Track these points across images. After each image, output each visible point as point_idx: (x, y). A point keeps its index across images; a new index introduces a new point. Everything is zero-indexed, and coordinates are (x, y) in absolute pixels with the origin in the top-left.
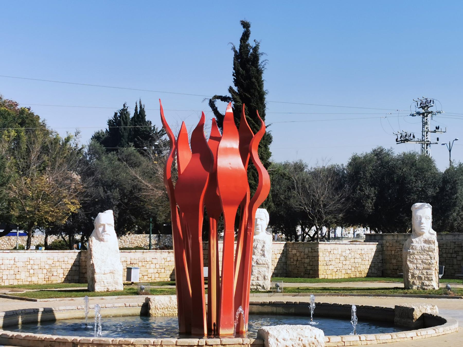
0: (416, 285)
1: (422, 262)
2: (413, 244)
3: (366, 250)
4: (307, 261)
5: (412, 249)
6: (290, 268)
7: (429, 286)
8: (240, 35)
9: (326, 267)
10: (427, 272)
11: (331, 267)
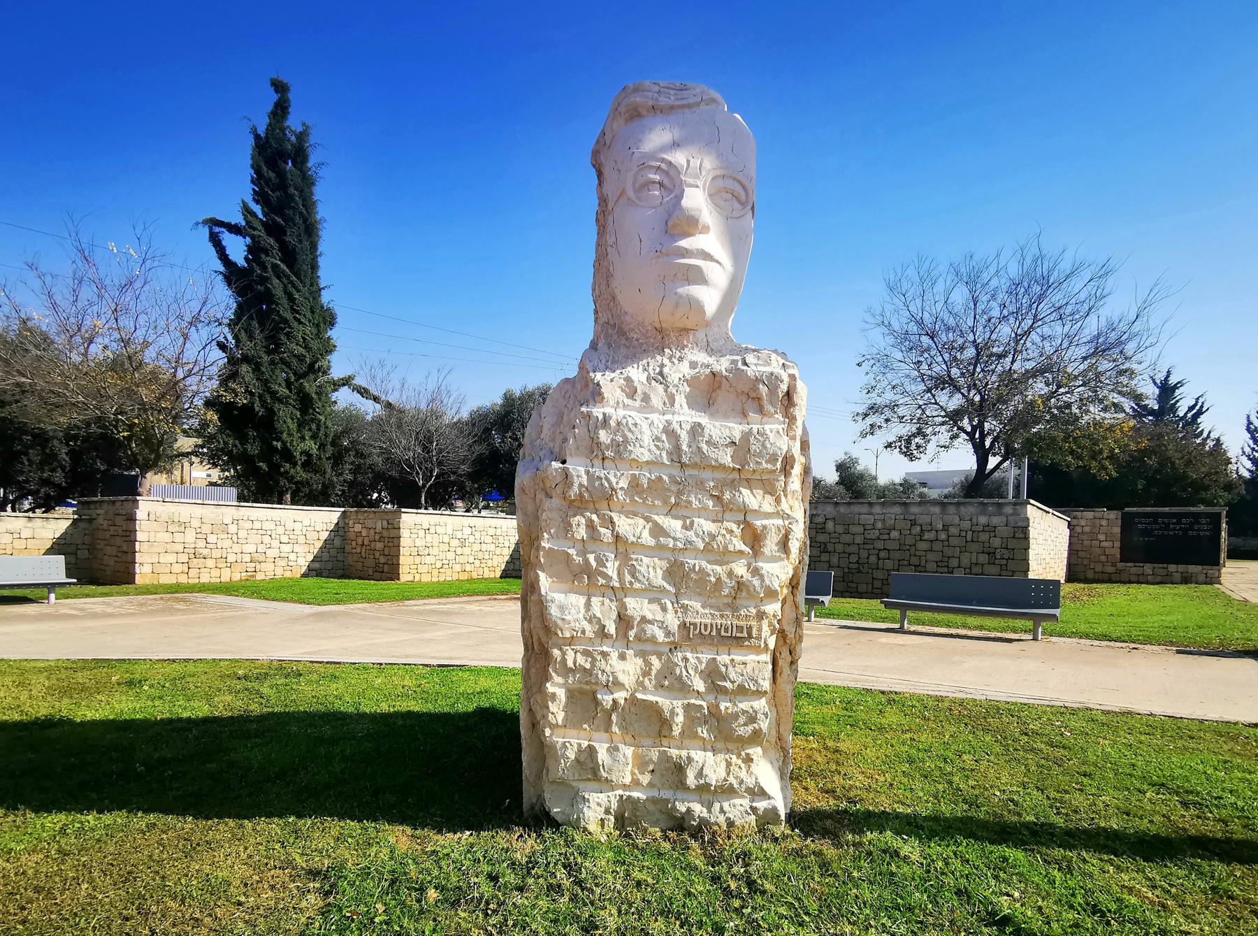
0: (609, 785)
1: (675, 572)
2: (598, 412)
3: (504, 529)
4: (379, 546)
5: (594, 450)
6: (350, 560)
7: (727, 791)
8: (270, 107)
9: (418, 560)
10: (713, 675)
11: (428, 560)
